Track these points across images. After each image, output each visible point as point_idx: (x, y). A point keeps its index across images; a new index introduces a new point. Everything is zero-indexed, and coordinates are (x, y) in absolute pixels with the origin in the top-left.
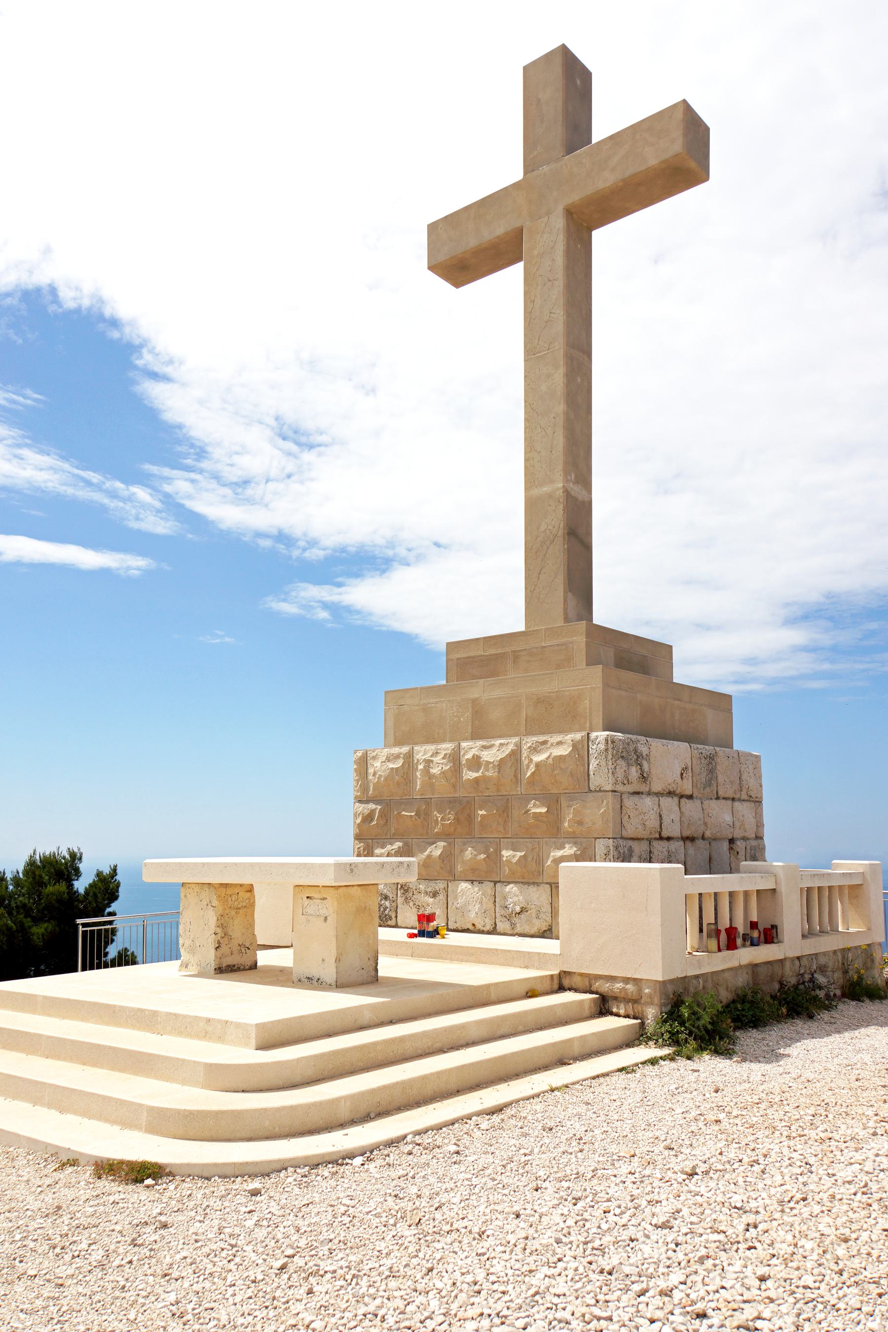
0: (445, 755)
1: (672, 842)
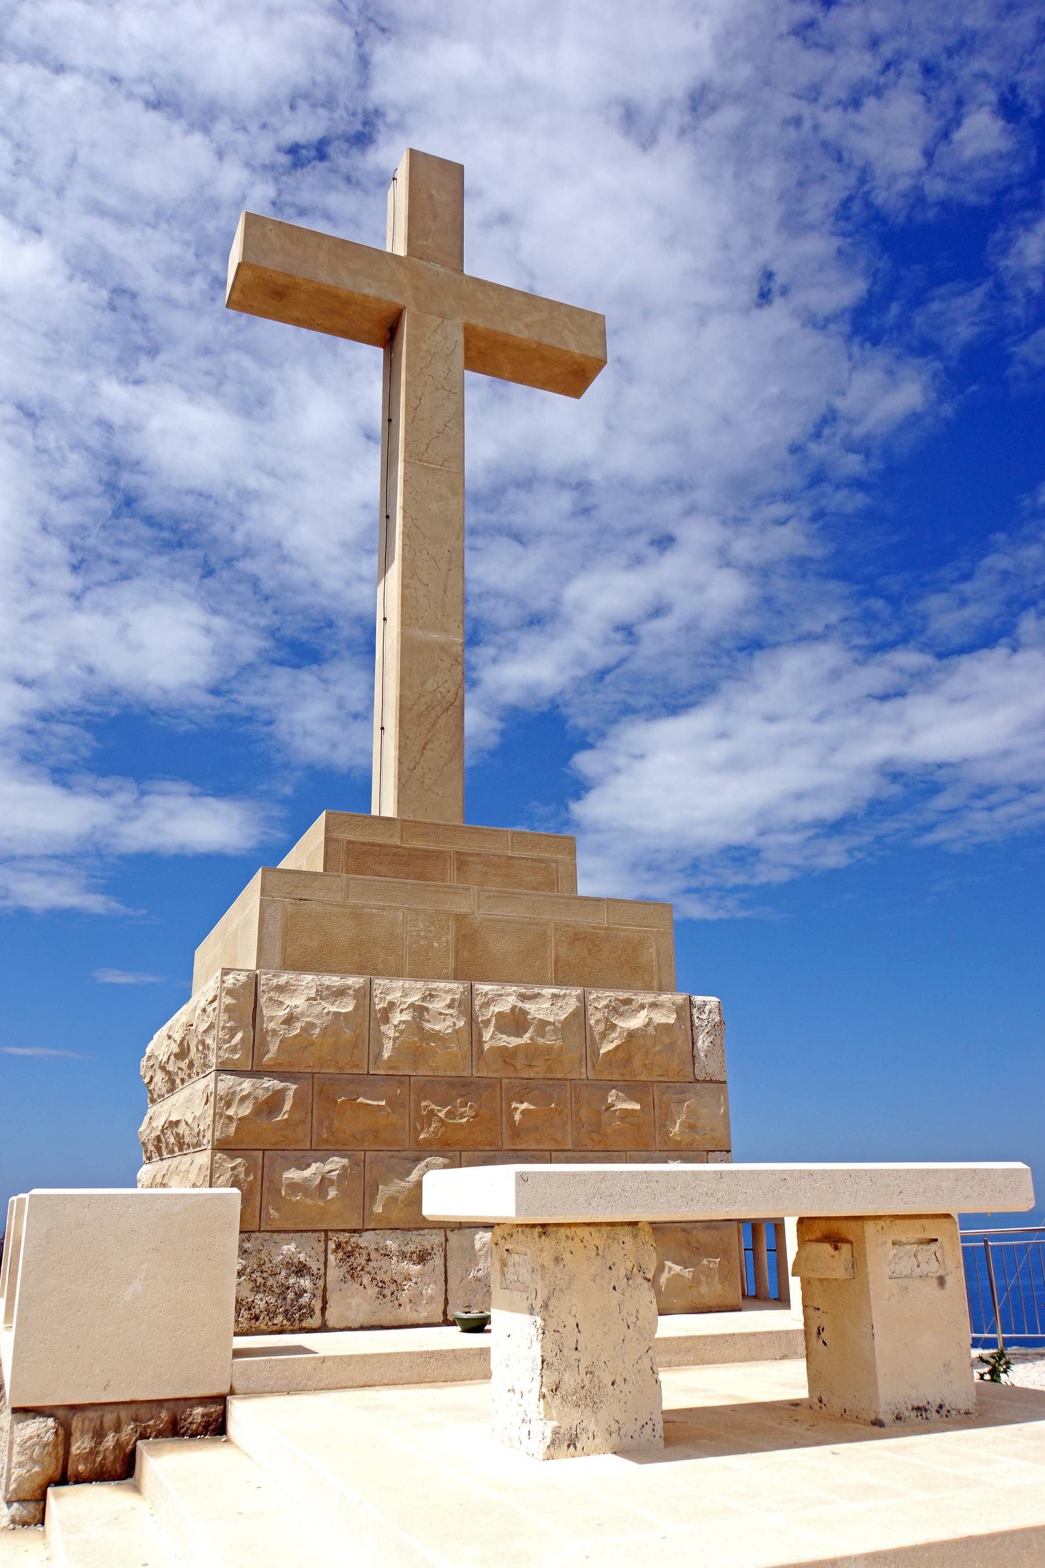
0: (453, 1000)
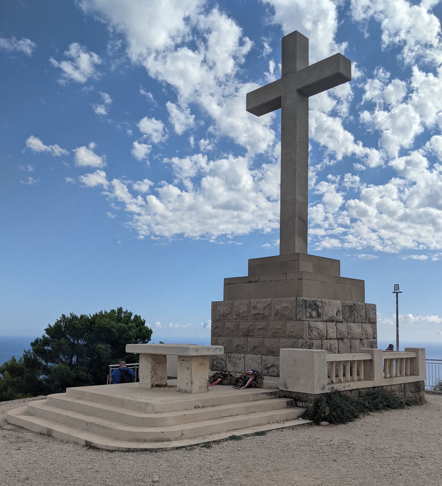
1: (332, 340)
